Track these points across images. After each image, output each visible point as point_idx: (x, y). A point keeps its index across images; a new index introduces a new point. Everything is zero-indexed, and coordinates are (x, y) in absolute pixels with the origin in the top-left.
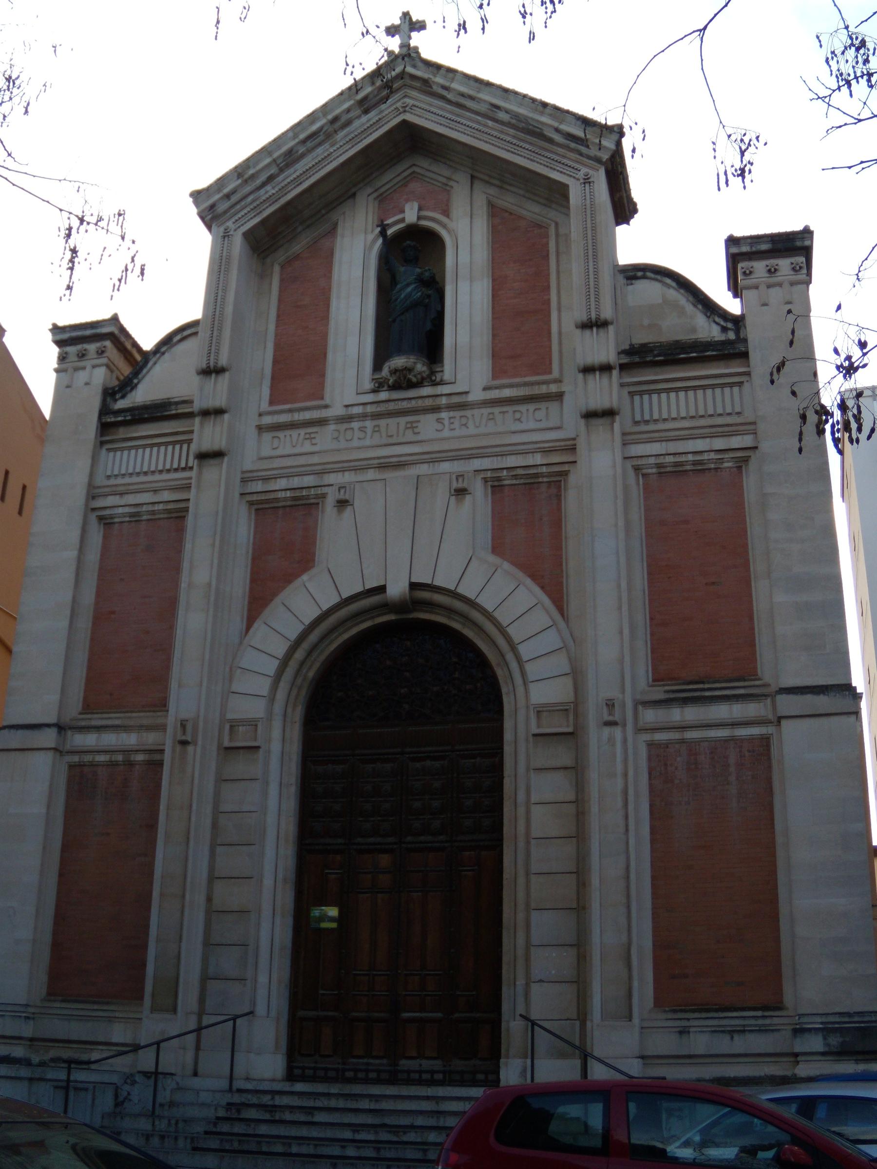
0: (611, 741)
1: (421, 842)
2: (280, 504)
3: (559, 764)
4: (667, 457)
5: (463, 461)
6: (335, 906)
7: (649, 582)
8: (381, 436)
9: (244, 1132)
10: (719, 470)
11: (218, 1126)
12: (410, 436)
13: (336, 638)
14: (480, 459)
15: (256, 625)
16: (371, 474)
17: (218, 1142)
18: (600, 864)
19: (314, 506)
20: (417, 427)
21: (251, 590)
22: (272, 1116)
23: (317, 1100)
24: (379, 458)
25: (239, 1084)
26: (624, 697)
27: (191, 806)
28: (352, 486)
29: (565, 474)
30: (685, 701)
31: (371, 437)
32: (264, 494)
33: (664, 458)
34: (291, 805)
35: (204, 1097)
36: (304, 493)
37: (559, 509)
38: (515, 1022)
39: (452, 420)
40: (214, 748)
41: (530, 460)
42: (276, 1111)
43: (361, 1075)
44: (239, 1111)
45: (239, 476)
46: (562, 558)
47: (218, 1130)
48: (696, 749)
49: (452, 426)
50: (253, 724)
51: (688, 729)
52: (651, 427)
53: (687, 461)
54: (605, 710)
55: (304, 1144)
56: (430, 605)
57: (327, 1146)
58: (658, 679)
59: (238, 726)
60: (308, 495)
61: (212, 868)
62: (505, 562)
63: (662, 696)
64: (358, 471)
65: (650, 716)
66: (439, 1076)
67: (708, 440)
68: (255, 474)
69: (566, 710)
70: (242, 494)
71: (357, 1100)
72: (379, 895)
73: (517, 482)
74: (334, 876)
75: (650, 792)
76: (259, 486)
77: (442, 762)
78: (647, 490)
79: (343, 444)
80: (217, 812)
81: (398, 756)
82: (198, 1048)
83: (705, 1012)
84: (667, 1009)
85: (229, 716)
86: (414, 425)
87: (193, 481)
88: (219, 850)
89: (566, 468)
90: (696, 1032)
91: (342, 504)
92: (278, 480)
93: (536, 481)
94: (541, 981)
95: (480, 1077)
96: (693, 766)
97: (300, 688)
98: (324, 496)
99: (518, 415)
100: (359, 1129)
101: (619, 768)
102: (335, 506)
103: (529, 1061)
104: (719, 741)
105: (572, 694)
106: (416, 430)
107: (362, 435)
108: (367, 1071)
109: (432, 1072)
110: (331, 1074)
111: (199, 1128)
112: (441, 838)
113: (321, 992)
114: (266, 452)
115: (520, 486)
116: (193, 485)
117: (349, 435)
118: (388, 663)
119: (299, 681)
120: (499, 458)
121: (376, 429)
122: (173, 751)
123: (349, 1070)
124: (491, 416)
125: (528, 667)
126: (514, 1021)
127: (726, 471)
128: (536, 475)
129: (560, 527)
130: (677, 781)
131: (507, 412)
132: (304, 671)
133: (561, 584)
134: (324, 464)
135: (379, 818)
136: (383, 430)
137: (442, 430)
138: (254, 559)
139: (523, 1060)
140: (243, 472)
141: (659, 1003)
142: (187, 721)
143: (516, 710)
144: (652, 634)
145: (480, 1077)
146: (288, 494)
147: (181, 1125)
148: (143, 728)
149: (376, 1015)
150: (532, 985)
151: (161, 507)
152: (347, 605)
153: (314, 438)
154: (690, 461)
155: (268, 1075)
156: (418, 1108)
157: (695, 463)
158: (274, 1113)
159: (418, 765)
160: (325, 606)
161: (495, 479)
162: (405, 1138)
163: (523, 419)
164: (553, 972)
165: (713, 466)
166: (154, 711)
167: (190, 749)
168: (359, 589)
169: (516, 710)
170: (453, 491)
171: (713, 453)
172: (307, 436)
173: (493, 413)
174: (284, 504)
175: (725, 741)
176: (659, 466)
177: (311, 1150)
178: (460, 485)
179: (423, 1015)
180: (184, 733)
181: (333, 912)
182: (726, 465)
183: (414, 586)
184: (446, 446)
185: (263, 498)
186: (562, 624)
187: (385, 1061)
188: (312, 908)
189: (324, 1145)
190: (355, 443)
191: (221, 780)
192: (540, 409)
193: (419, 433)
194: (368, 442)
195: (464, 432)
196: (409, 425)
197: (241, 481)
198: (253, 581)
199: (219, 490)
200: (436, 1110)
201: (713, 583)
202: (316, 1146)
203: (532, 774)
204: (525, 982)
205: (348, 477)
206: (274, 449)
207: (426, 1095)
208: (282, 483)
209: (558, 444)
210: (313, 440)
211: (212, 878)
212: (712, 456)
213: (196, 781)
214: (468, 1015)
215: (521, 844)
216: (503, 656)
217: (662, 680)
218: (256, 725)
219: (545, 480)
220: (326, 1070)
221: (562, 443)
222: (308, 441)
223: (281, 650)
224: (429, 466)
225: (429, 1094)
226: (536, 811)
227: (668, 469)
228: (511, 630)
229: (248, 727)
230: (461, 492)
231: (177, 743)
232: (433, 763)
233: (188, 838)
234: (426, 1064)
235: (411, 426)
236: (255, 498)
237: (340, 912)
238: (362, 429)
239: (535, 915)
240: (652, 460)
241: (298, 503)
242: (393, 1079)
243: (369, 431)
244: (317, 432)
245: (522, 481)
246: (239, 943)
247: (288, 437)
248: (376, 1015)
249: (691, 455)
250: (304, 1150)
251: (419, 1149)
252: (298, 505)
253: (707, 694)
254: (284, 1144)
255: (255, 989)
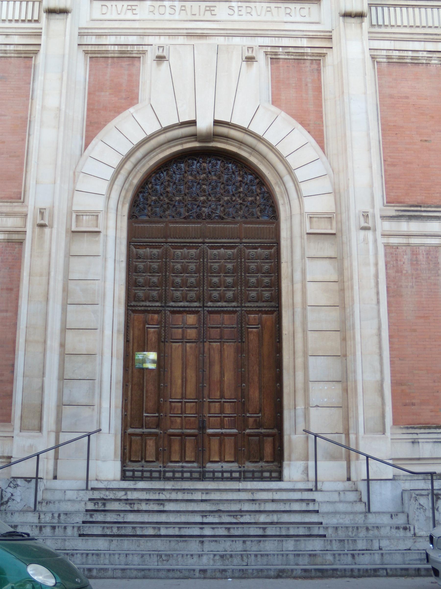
0: (365, 241)
1: (219, 307)
2: (110, 55)
3: (326, 254)
4: (394, 51)
5: (250, 38)
6: (154, 351)
7: (382, 136)
8: (187, 14)
9: (116, 520)
10: (429, 65)
11: (93, 516)
12: (208, 16)
13: (154, 156)
14: (262, 38)
15: (93, 142)
16: (181, 40)
17: (101, 529)
18: (361, 325)
19: (136, 59)
20: (214, 10)
21: (88, 116)
22: (131, 507)
23: (161, 494)
24: (186, 29)
25: (93, 484)
26: (374, 211)
27: (49, 273)
28: (168, 47)
29: (324, 55)
30: (410, 218)
31: (179, 14)
32: (97, 46)
33: (393, 52)
34: (122, 276)
35: (70, 495)
36: (129, 48)
37: (319, 79)
38: (297, 436)
39: (240, 9)
40: (64, 232)
41: (299, 43)
42: (134, 504)
43: (178, 475)
44: (104, 505)
45: (76, 32)
46: (322, 113)
47: (94, 520)
48: (416, 251)
49: (240, 13)
50: (95, 215)
51: (412, 237)
52: (389, 30)
53: (407, 56)
54: (362, 219)
55: (171, 527)
56: (227, 138)
57: (189, 528)
58: (390, 202)
59: (83, 216)
60: (132, 51)
61: (64, 321)
62: (283, 112)
63: (394, 214)
64: (171, 37)
65: (388, 226)
66: (236, 475)
67: (423, 43)
68: (90, 31)
69: (330, 218)
70: (79, 45)
71: (192, 493)
72: (188, 344)
73: (289, 57)
74: (152, 330)
75: (386, 278)
76: (93, 40)
77: (232, 251)
78: (380, 74)
79: (157, 17)
80: (67, 280)
81: (200, 245)
82: (56, 458)
83: (427, 429)
84: (402, 427)
85: (75, 208)
86: (212, 9)
87: (43, 31)
88: (69, 308)
89: (324, 51)
90: (423, 442)
91: (160, 59)
92: (108, 37)
93: (303, 58)
94: (317, 406)
95: (267, 474)
96: (415, 262)
97: (127, 191)
98: (144, 53)
99: (288, 11)
100: (206, 514)
101: (372, 259)
102: (154, 60)
103: (311, 463)
104: (433, 246)
105: (334, 206)
106: (213, 13)
107: (172, 11)
108: (182, 472)
109: (231, 472)
110: (156, 475)
111: (79, 519)
112: (234, 304)
113: (145, 415)
114: (97, 15)
115: (291, 60)
116: (43, 34)
117: (162, 10)
118: (190, 177)
119: (127, 186)
120: (277, 39)
121: (183, 8)
122: (33, 232)
123: (187, 472)
124: (269, 9)
125: (303, 186)
126: (295, 434)
127: (433, 66)
128: (303, 54)
129: (321, 92)
130: (404, 272)
131: (281, 7)
132: (131, 179)
133: (322, 131)
134: (145, 29)
135: (186, 289)
136: (188, 10)
137: (232, 15)
138: (89, 94)
139: (305, 462)
140: (80, 28)
141: (395, 422)
142: (45, 209)
143: (291, 216)
144: (385, 171)
145: (267, 474)
146: (116, 48)
147: (62, 517)
148: (3, 214)
149: (189, 431)
150: (311, 409)
151: (12, 48)
152: (164, 133)
153: (135, 9)
154: (410, 56)
155: (111, 477)
156: (239, 498)
157: (413, 58)
158: (133, 505)
159: (215, 252)
160: (149, 133)
161: (273, 54)
162: (242, 520)
163: (292, 14)
164: (326, 400)
165: (424, 61)
166: (11, 202)
167: (47, 230)
168: (175, 121)
169: (291, 216)
170: (244, 60)
171: (426, 52)
172: (129, 8)
173: (270, 7)
174: (112, 55)
175: (436, 247)
176: (388, 57)
177: (176, 532)
178: (250, 54)
179: (223, 431)
180: (42, 219)
181: (153, 355)
182: (433, 62)
183: (217, 123)
184: (236, 26)
185: (93, 49)
186: (324, 158)
187: (195, 465)
188: (136, 353)
189: (186, 528)
190: (167, 17)
191: (69, 255)
192: (304, 8)
193: (215, 15)
194: (177, 17)
195: (249, 18)
196: (208, 9)
197: (79, 35)
198: (90, 110)
199: (65, 39)
200: (251, 499)
201: (426, 141)
202: (180, 528)
203: (308, 262)
204: (304, 407)
205: (163, 41)
206: (103, 14)
207: (238, 488)
208: (112, 40)
209: (319, 34)
210: (134, 11)
211: (64, 329)
212: (425, 54)
213: (53, 255)
214: (256, 430)
215: (298, 309)
216: (281, 178)
217: (393, 203)
218: (97, 216)
219: (309, 58)
220: (151, 472)
221: (322, 34)
222: (130, 11)
223: (116, 161)
224: (225, 38)
225: (241, 487)
226: (310, 287)
227: (394, 60)
228: (289, 159)
229: (90, 217)
230: (250, 59)
231: (36, 225)
232: (226, 250)
233: (48, 299)
234: (227, 466)
235: (210, 9)
236: (89, 48)
237: (159, 356)
238: (172, 7)
239: (311, 360)
240: (384, 53)
241: (123, 55)
242: (202, 477)
243: (178, 9)
244: (137, 6)
245: (292, 57)
246: (88, 378)
247: (114, 6)
248: (189, 431)
249: (411, 52)
250: (171, 532)
251: (260, 528)
252: (124, 57)
253: (424, 214)
254: (154, 528)
255: (100, 413)
